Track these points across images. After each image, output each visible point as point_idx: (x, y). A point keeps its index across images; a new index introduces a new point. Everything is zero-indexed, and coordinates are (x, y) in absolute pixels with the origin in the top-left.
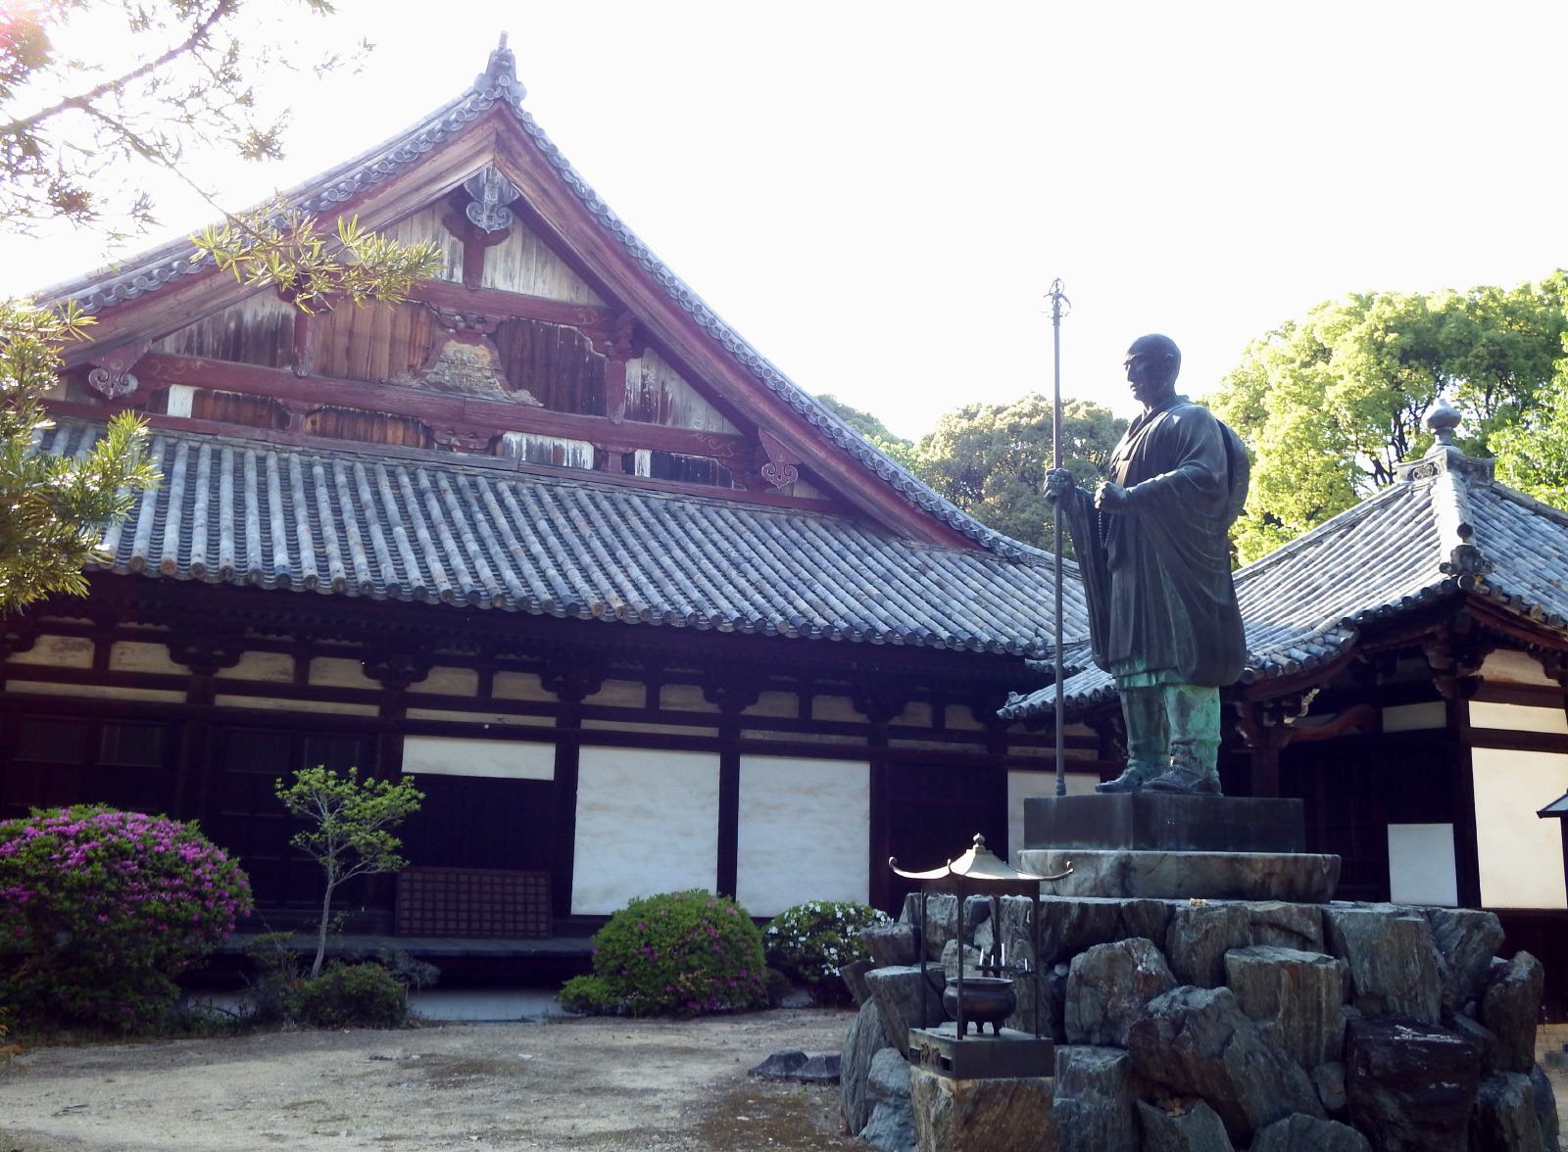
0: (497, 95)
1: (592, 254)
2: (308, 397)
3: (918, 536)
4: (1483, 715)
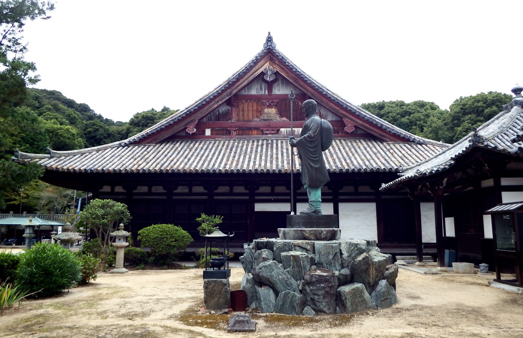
0: (268, 47)
1: (295, 81)
2: (235, 127)
3: (391, 140)
4: (505, 182)
